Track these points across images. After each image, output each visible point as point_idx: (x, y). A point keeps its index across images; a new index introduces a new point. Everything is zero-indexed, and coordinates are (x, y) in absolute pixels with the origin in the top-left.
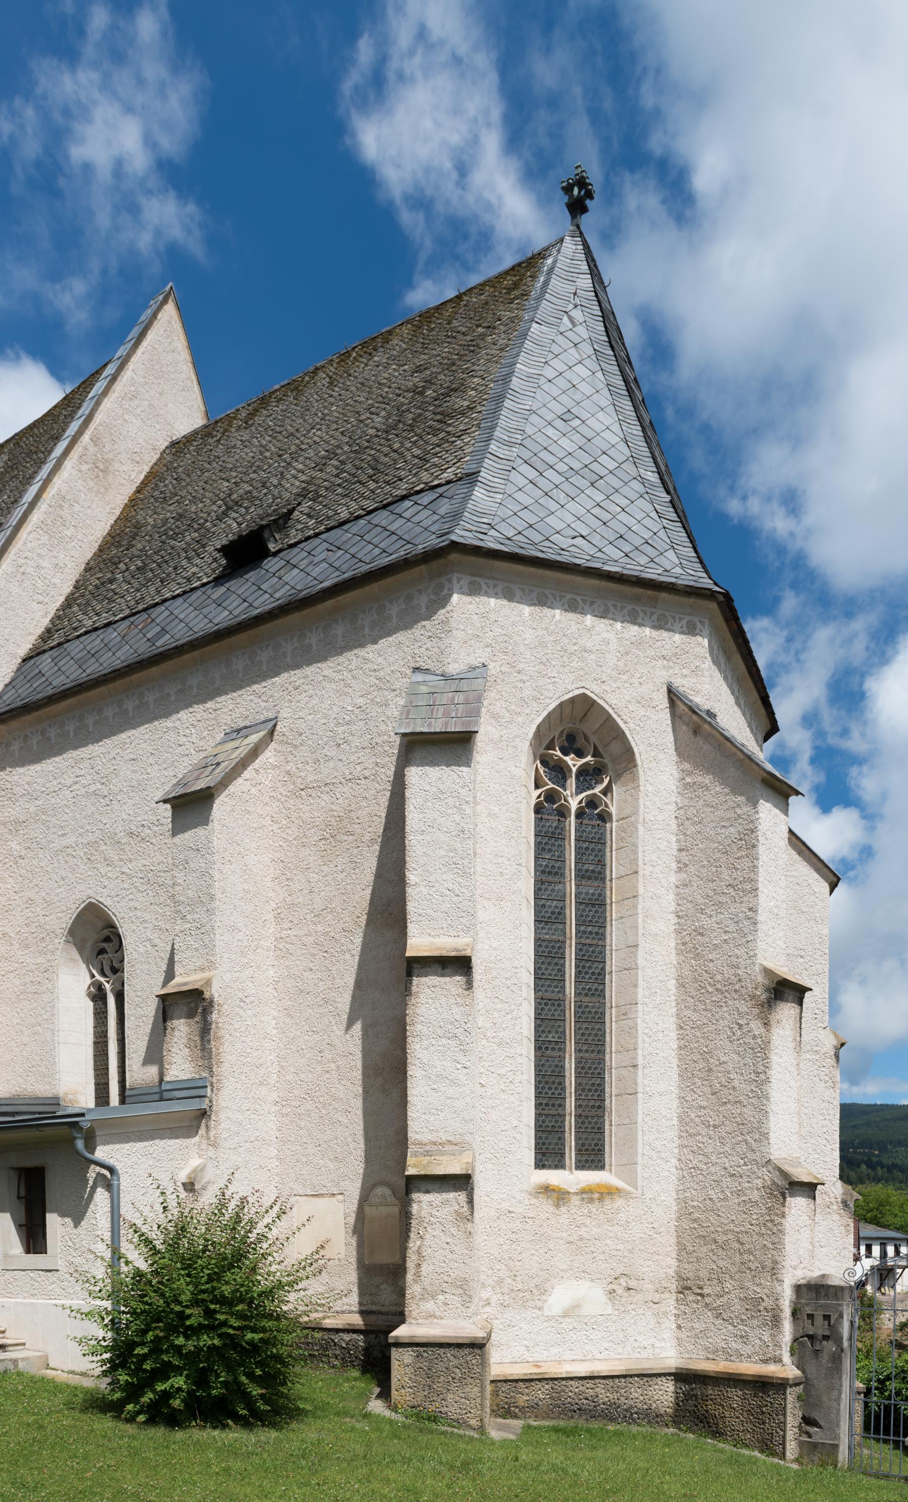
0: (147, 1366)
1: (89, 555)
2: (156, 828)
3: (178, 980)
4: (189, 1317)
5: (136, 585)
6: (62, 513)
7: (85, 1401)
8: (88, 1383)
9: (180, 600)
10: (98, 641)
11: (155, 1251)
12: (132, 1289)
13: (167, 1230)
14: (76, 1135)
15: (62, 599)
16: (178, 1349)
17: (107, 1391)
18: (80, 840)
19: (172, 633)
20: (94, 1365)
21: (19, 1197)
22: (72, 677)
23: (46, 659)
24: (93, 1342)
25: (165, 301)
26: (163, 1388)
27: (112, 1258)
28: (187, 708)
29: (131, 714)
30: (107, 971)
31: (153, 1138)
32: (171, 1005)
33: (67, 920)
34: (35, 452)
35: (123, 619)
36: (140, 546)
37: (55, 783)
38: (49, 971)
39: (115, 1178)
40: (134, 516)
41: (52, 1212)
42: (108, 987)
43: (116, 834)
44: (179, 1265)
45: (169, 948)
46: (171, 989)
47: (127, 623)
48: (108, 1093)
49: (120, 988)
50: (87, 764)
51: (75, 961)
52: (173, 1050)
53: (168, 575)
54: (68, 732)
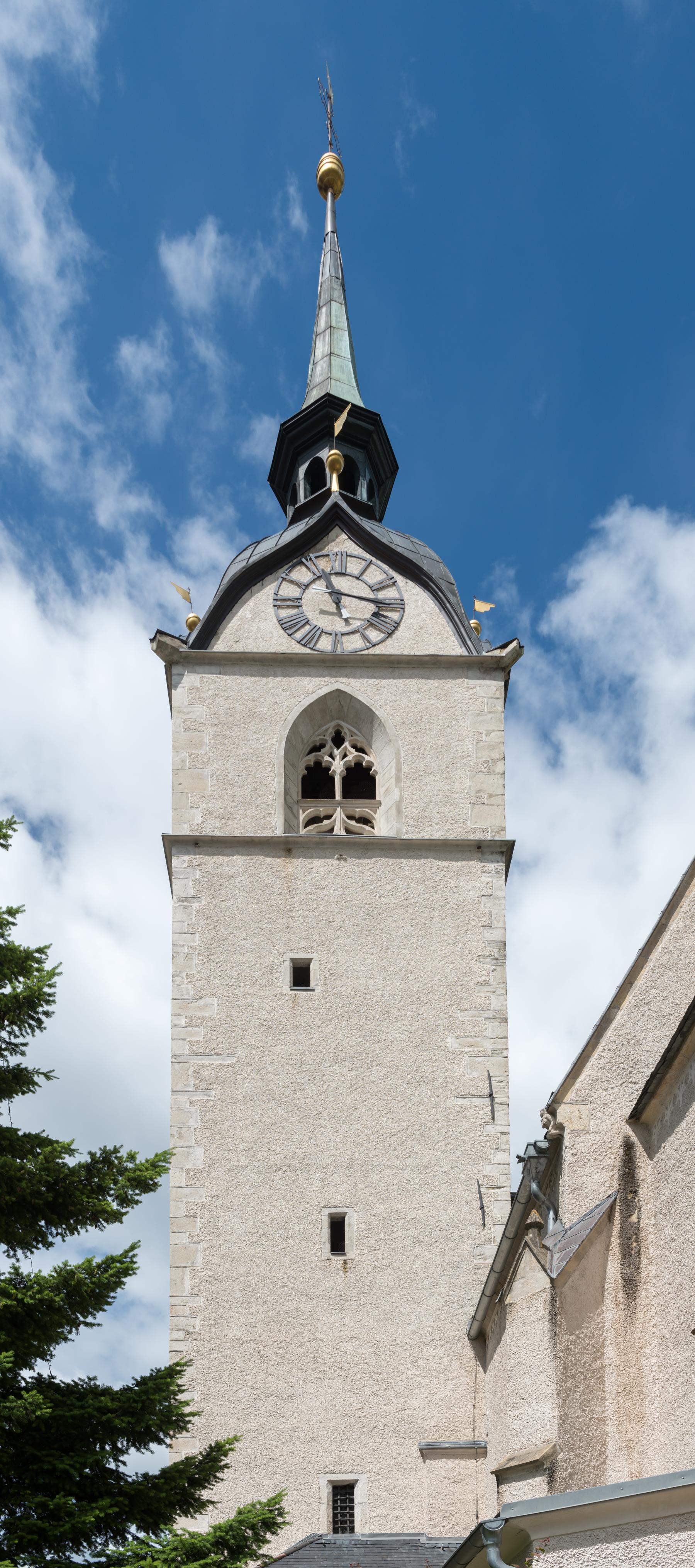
31: (644, 1533)
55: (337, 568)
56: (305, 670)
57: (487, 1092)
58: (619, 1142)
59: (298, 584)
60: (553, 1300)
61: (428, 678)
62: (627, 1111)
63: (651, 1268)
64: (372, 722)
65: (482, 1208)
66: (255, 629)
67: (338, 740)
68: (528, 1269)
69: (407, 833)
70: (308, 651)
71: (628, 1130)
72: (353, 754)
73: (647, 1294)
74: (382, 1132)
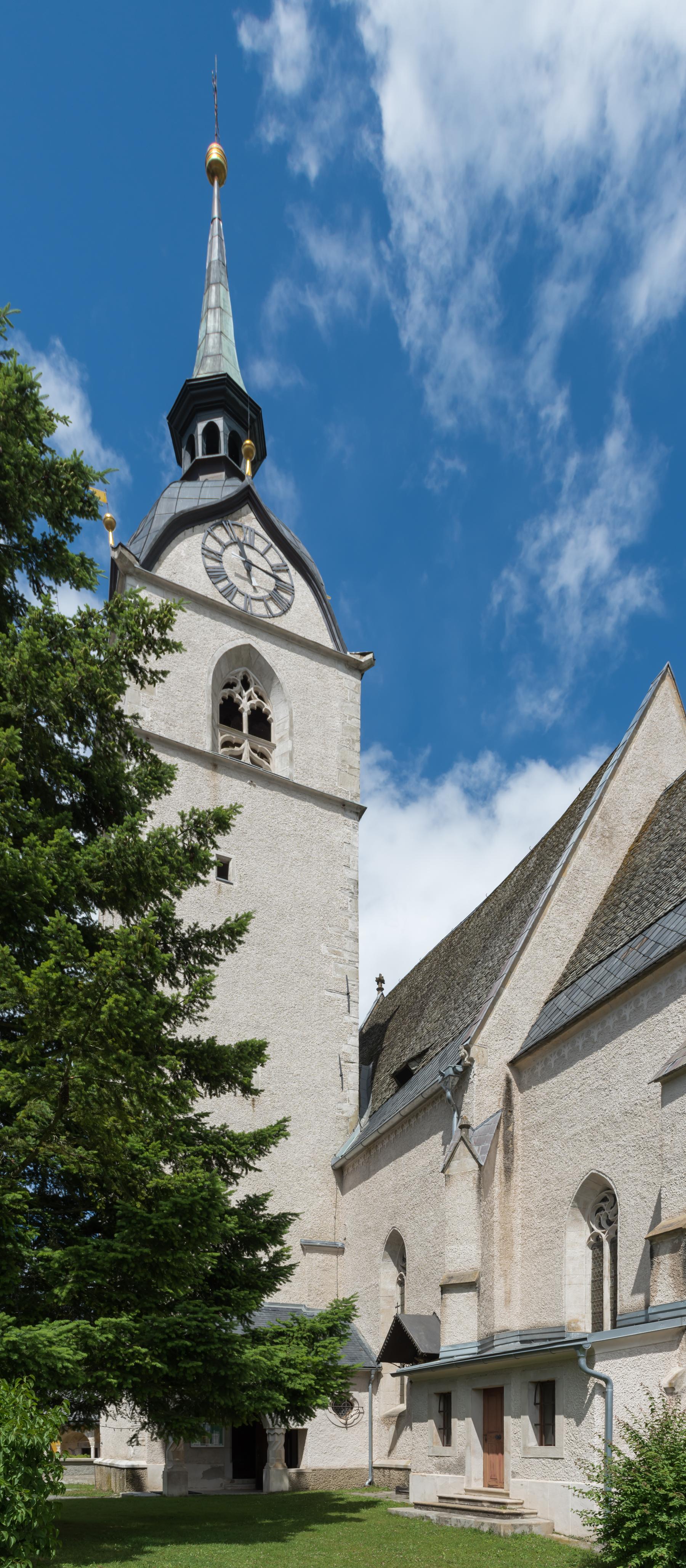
0: (635, 1537)
1: (595, 908)
2: (647, 1104)
3: (663, 1222)
4: (672, 1499)
5: (634, 915)
6: (576, 883)
7: (583, 1560)
8: (583, 1546)
9: (672, 913)
10: (603, 969)
11: (643, 1445)
12: (624, 1475)
13: (653, 1427)
14: (579, 1355)
15: (575, 947)
16: (662, 1525)
17: (600, 1555)
18: (585, 1127)
19: (663, 943)
20: (592, 1533)
21: (535, 1404)
22: (581, 1005)
23: (563, 996)
24: (590, 1515)
25: (663, 679)
26: (648, 1555)
27: (606, 1450)
28: (676, 999)
29: (628, 1019)
30: (604, 1224)
31: (641, 1353)
32: (658, 1244)
33: (574, 1190)
34: (557, 846)
35: (622, 946)
36: (637, 884)
37: (567, 1088)
38: (559, 1232)
39: (609, 1386)
40: (633, 862)
41: (560, 1414)
42: (604, 1236)
43: (613, 1116)
44: (663, 1456)
45: (655, 1198)
46: (657, 1231)
47: (626, 948)
48: (602, 1319)
49: (614, 1236)
50: (592, 1067)
51: (577, 1220)
52: (659, 1280)
53: (661, 898)
54: (578, 1047)
55: (248, 541)
56: (227, 619)
57: (345, 991)
58: (503, 1077)
59: (220, 542)
60: (479, 1179)
61: (312, 659)
62: (510, 1057)
63: (519, 1162)
64: (272, 679)
65: (341, 1075)
66: (188, 568)
67: (246, 685)
68: (462, 1154)
69: (296, 778)
70: (227, 603)
71: (508, 1070)
72: (256, 700)
73: (517, 1178)
74: (278, 1006)
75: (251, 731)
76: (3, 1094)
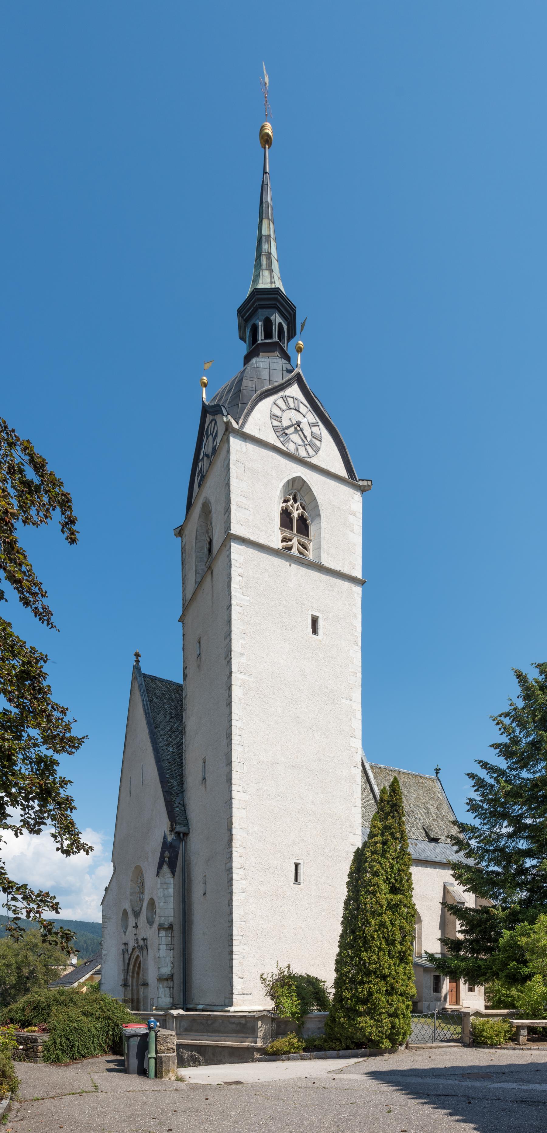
72: (301, 510)
75: (298, 531)
76: (3, 797)
